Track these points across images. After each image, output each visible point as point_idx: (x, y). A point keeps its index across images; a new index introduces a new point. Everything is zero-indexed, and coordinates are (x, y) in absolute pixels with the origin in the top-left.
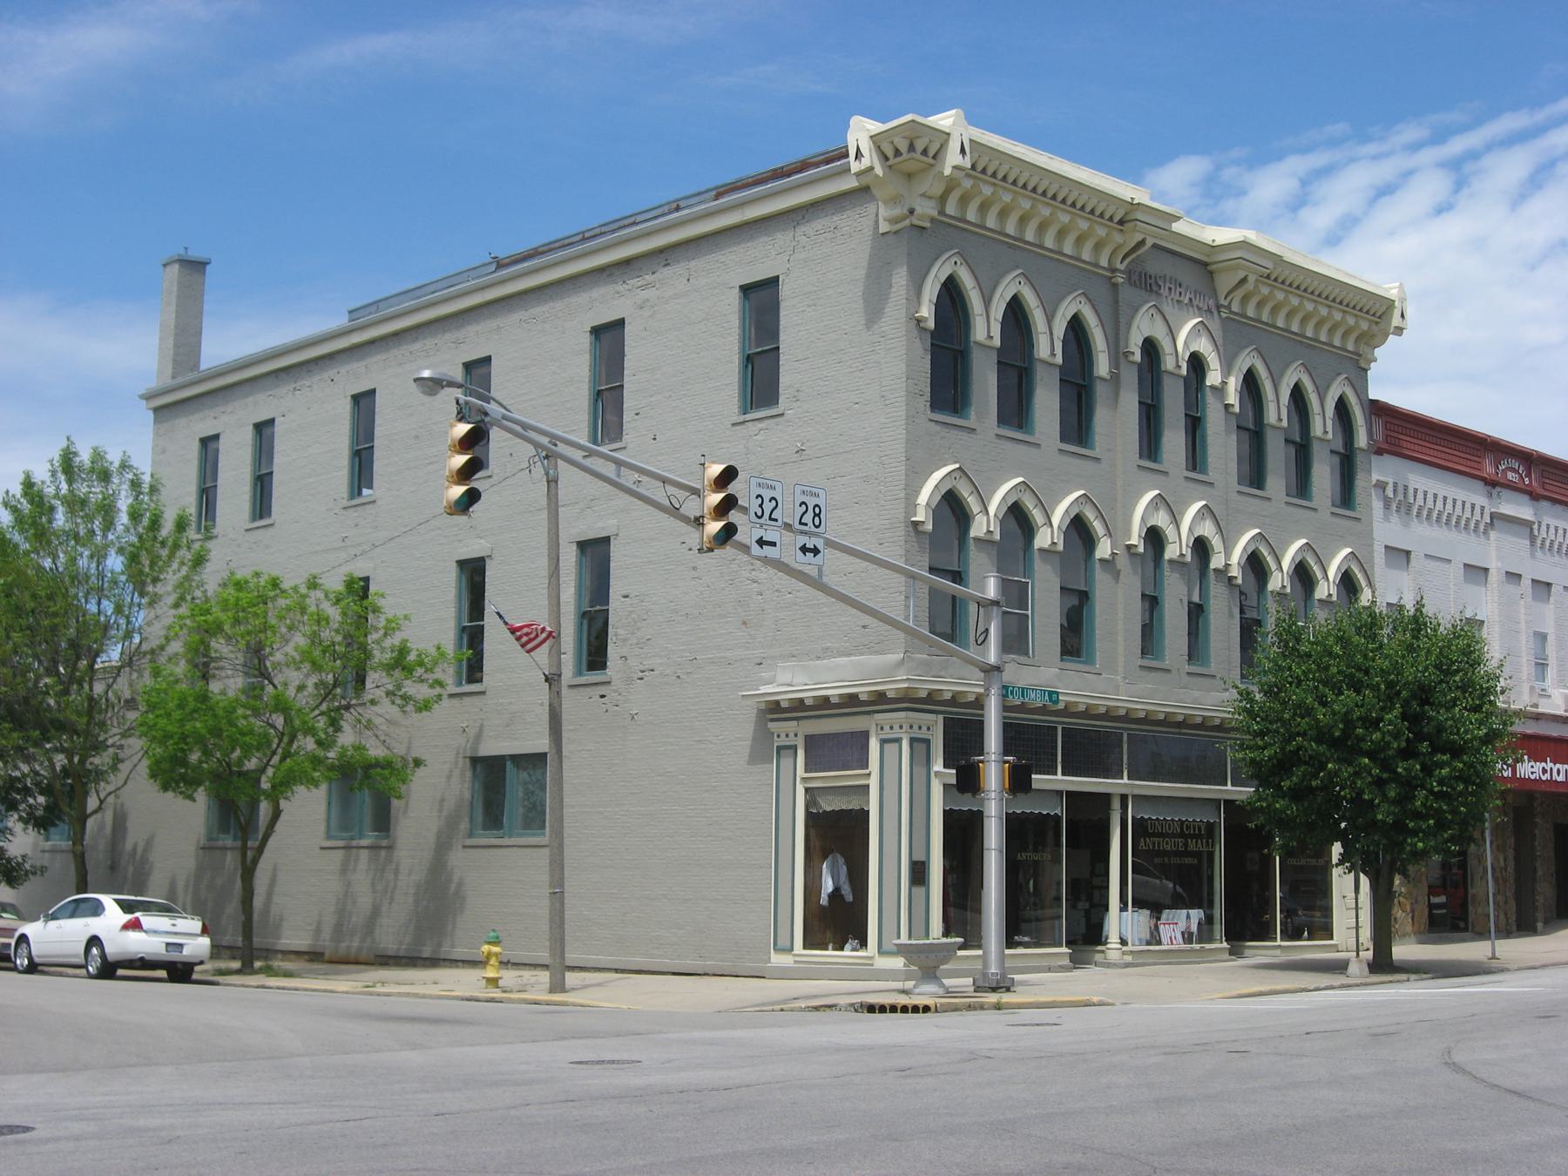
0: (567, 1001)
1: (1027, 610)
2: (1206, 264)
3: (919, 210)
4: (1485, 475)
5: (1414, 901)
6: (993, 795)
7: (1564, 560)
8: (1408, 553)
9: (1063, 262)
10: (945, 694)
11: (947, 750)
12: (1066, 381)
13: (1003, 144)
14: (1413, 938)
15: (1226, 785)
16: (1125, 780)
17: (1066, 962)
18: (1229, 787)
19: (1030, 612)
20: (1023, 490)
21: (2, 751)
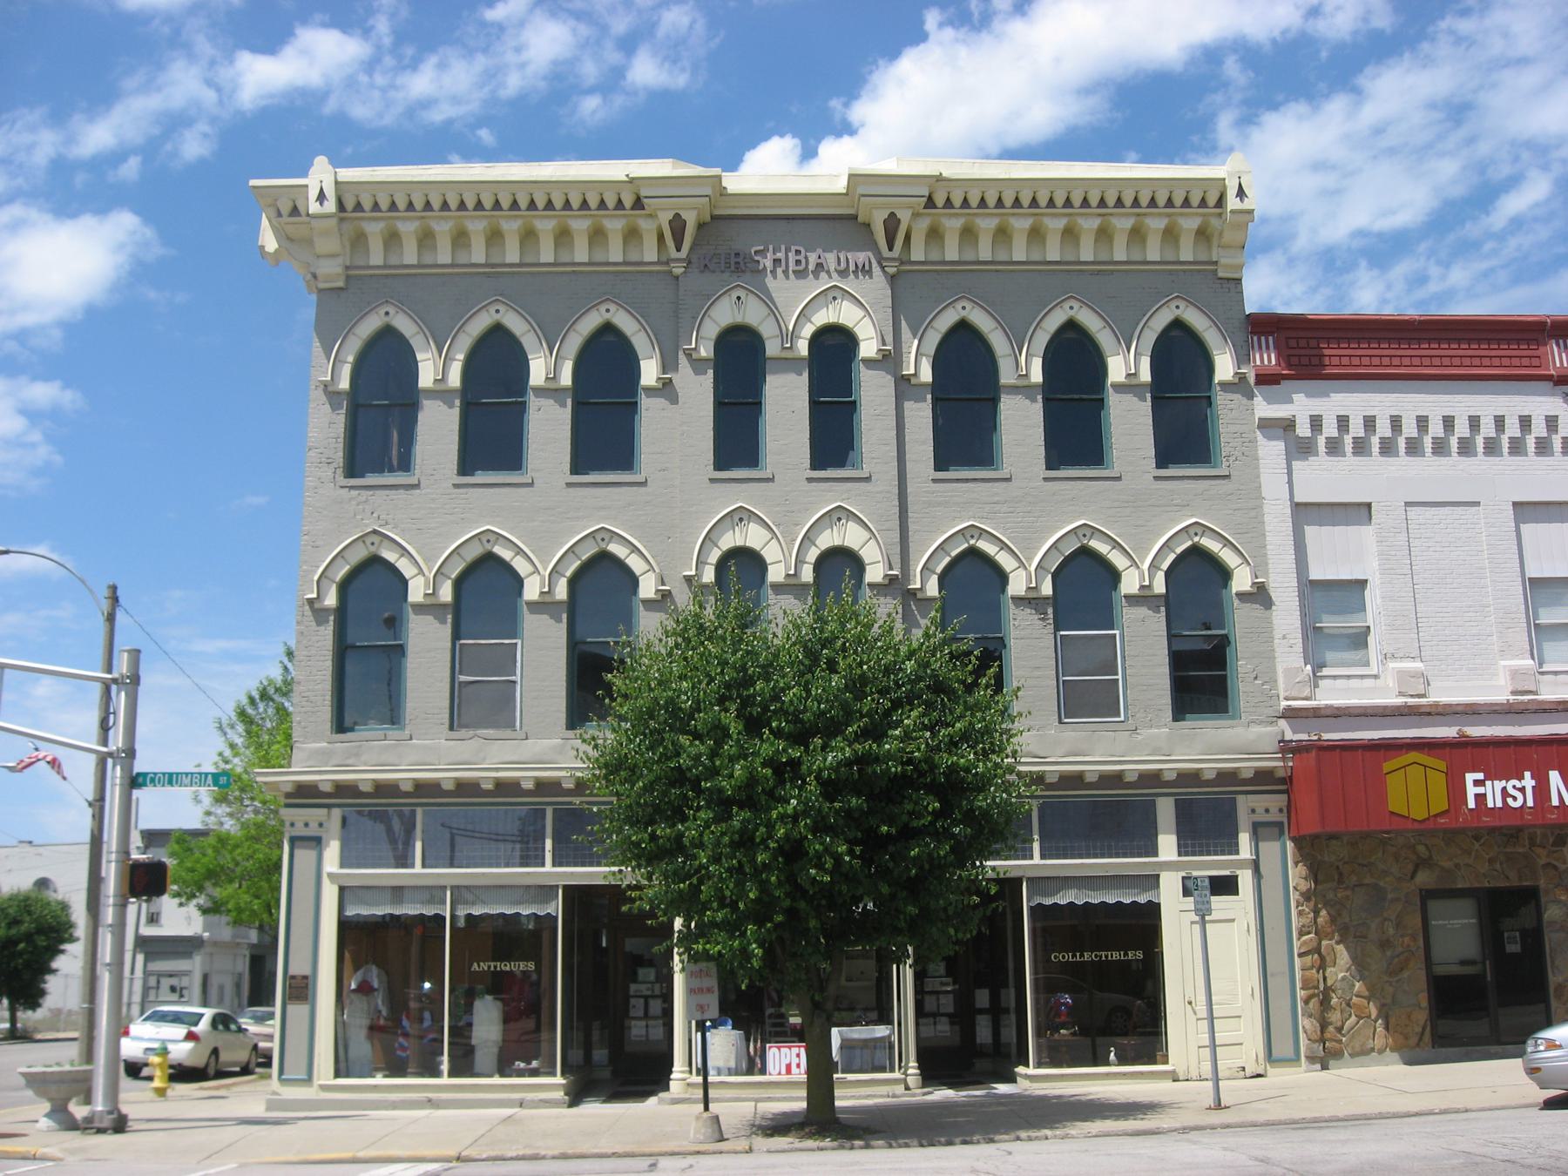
0: (538, 1154)
1: (1117, 674)
2: (855, 217)
3: (320, 272)
4: (1553, 372)
5: (1389, 1001)
6: (111, 901)
7: (1558, 459)
8: (1369, 505)
9: (581, 272)
10: (1394, 784)
11: (557, 853)
12: (942, 399)
13: (421, 172)
14: (1396, 1056)
15: (543, 865)
16: (548, 868)
17: (560, 1095)
18: (548, 868)
19: (1120, 677)
20: (1200, 533)
21: (11, 942)
